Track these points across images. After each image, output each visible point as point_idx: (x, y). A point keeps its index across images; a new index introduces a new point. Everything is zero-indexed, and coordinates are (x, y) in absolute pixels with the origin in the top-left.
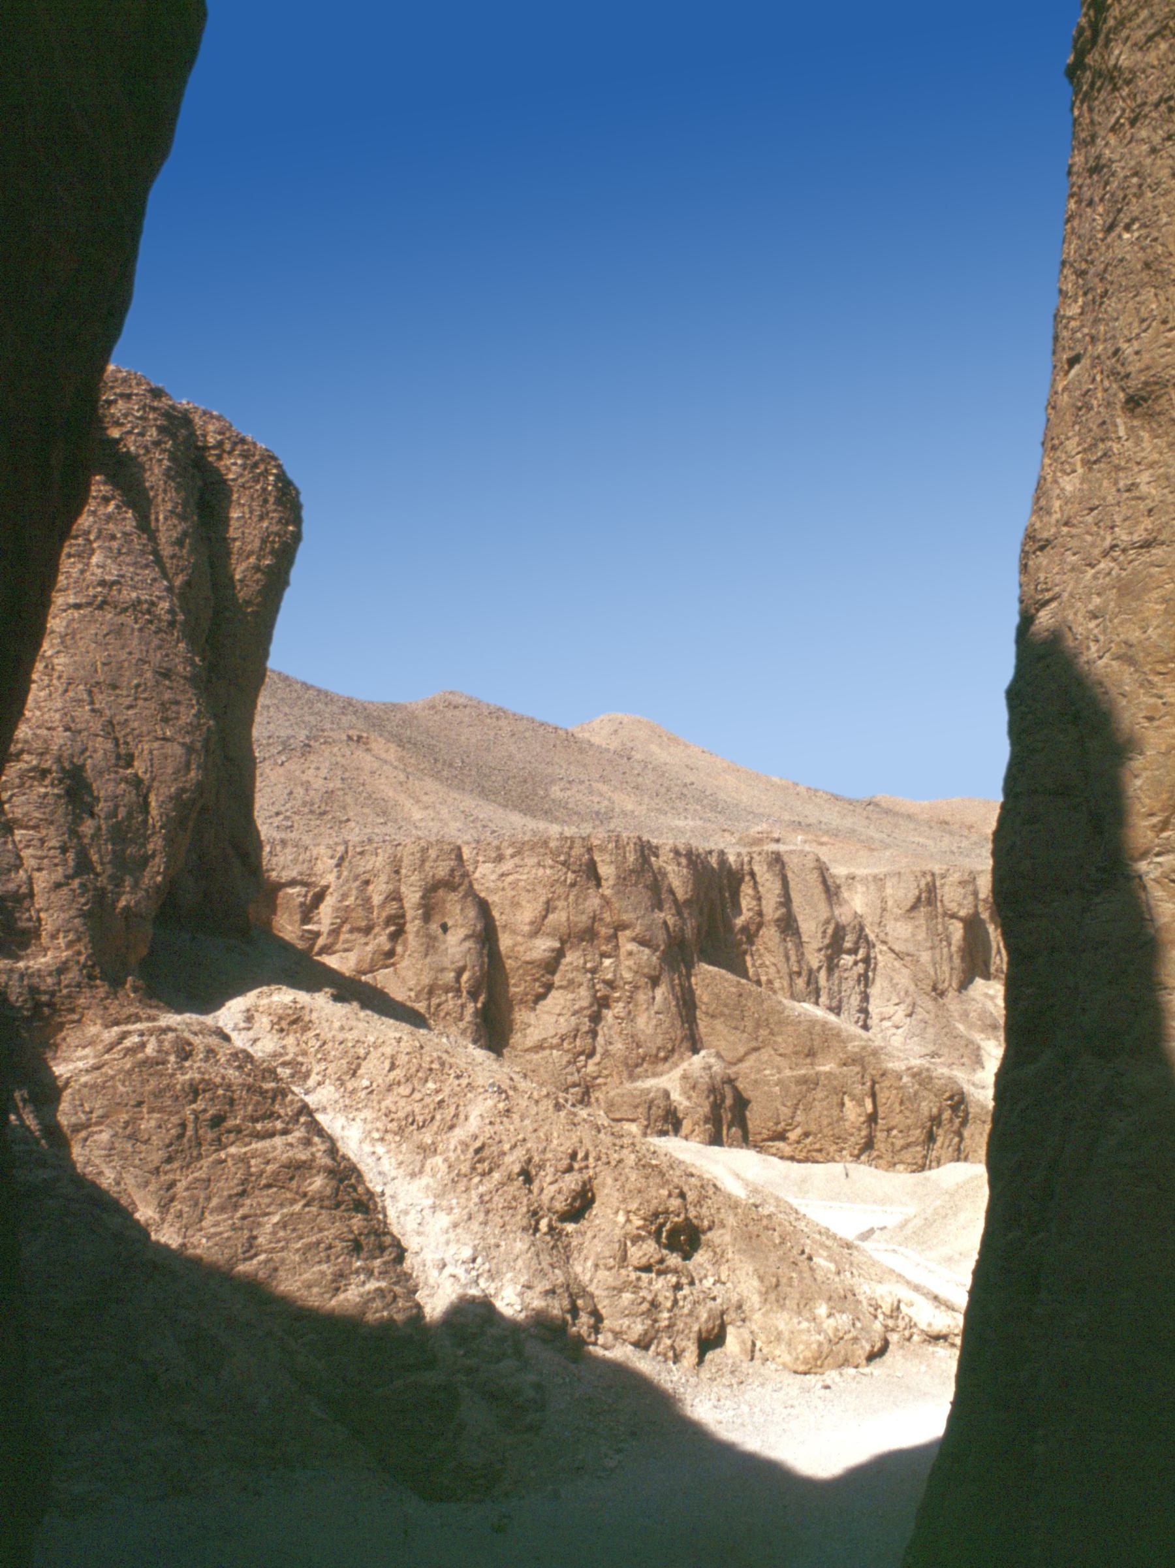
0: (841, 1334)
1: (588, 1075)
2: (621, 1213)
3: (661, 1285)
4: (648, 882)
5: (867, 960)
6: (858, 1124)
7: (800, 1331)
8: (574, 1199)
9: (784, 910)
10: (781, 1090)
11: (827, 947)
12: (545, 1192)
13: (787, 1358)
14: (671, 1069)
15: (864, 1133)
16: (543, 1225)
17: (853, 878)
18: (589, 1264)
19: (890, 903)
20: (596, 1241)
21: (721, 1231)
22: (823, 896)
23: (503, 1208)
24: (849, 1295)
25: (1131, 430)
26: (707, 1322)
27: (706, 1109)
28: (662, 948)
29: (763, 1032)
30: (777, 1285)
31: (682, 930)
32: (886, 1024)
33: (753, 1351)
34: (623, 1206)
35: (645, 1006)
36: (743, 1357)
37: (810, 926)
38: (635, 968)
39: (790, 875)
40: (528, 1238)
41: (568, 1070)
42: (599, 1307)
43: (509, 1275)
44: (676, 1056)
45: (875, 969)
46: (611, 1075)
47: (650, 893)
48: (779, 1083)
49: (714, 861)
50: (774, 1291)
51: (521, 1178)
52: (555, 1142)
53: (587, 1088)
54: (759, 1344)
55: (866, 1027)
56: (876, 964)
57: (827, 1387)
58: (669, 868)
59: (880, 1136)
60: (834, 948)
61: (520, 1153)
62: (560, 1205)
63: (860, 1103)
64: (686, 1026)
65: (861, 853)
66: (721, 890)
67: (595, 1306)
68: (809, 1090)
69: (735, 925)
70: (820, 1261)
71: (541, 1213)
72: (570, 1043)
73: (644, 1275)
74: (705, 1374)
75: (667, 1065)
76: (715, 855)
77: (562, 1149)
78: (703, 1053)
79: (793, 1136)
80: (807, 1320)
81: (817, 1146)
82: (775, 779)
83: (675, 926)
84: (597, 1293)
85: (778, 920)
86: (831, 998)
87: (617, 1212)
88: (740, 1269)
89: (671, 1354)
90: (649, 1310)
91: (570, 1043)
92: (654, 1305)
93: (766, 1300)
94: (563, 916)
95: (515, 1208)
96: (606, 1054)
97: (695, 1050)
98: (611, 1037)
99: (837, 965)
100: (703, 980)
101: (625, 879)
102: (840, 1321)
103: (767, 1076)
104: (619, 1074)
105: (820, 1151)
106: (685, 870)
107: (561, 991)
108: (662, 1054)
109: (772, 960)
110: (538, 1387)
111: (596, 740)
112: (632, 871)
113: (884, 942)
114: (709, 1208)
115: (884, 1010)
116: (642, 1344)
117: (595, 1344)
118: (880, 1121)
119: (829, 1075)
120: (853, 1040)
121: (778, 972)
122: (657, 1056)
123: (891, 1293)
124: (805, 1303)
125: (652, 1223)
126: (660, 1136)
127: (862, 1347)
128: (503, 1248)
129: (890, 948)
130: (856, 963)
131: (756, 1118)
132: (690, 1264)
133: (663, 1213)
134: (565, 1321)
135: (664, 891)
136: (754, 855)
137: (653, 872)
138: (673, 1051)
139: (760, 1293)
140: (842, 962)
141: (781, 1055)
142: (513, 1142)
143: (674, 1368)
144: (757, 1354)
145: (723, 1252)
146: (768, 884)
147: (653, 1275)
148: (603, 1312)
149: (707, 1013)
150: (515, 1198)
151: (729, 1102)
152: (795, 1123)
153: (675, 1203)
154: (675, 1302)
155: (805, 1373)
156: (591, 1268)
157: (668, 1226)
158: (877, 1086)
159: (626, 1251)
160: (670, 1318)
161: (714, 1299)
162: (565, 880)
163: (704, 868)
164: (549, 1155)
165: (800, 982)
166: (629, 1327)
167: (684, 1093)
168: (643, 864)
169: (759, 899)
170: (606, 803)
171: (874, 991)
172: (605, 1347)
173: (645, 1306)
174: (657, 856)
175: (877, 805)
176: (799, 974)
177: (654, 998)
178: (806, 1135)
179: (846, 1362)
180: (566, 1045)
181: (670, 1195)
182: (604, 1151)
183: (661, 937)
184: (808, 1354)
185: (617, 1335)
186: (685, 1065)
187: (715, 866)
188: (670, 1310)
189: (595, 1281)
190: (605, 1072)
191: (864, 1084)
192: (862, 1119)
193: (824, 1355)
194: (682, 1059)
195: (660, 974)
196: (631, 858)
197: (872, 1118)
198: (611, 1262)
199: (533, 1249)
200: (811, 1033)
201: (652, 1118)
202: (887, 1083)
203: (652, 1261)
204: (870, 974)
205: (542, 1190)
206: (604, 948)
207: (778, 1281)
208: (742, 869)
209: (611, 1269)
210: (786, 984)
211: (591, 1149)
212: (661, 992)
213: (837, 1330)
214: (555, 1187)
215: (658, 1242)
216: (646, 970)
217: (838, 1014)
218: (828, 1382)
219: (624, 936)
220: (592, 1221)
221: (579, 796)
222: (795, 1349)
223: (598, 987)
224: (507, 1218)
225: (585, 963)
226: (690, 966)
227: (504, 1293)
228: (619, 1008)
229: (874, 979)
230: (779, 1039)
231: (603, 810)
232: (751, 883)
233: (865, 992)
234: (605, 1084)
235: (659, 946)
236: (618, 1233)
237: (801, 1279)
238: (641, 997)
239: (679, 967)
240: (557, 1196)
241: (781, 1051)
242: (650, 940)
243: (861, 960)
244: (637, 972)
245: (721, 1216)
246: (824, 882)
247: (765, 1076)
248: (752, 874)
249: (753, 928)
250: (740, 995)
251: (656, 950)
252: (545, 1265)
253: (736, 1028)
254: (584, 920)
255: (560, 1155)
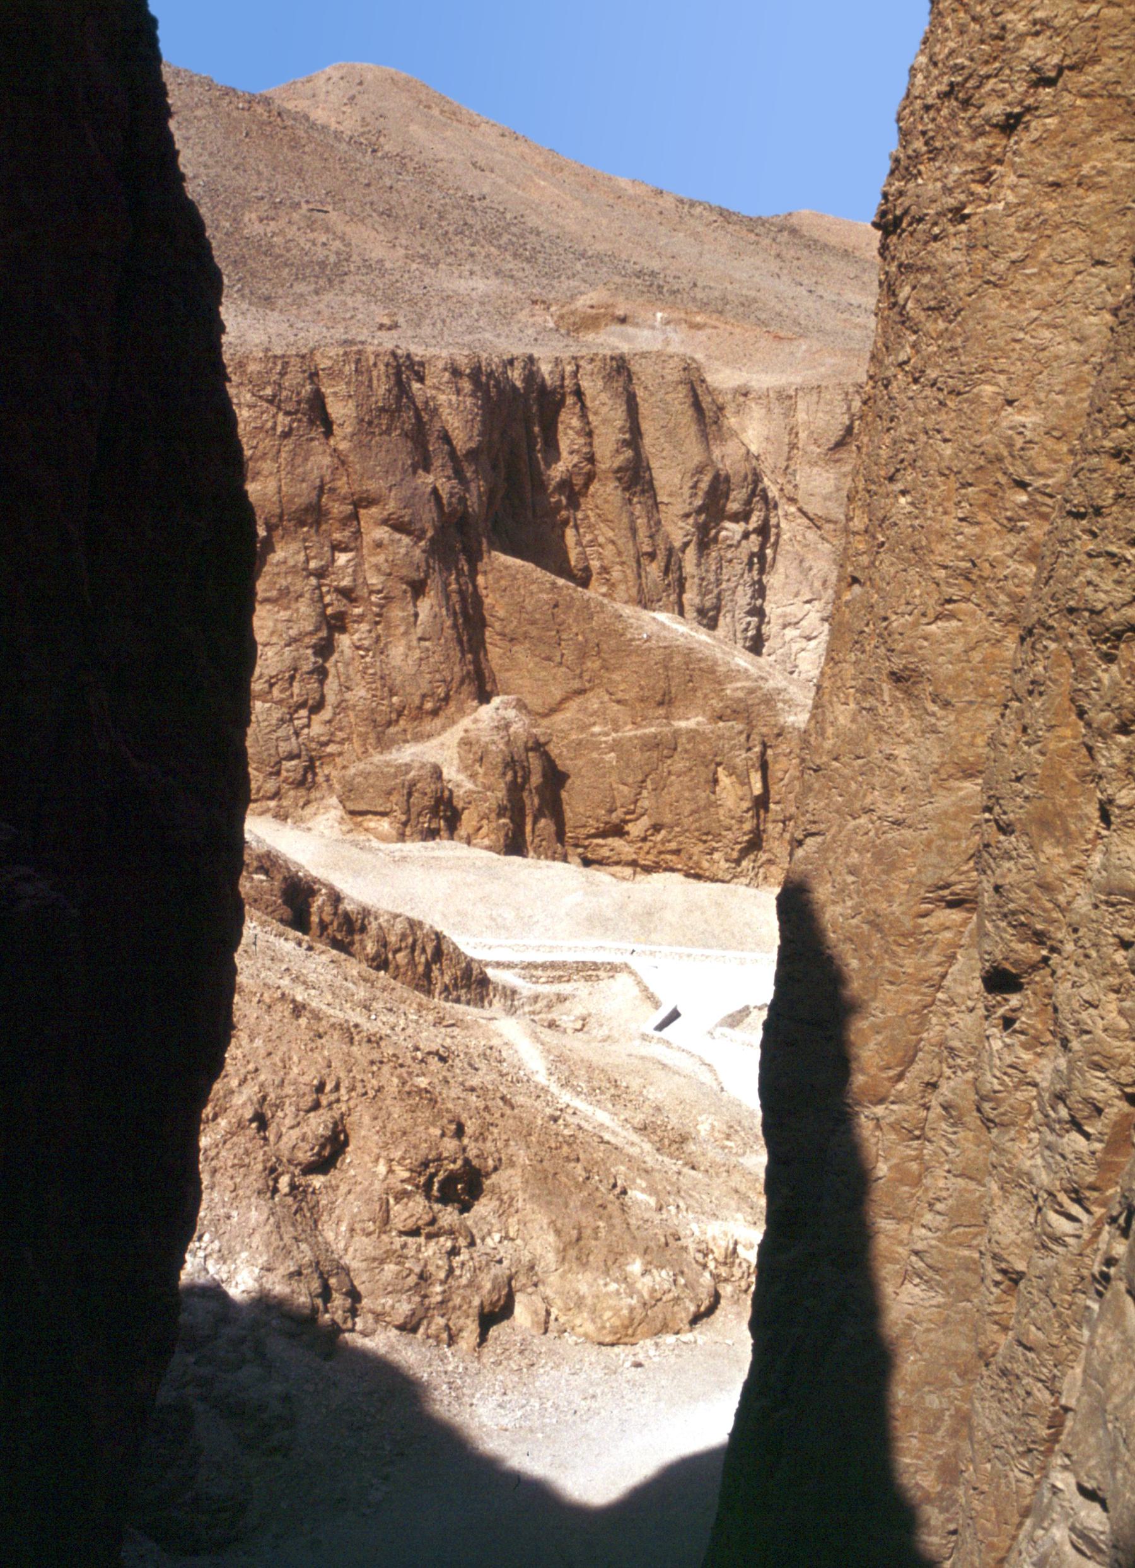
0: (658, 1295)
1: (312, 740)
2: (382, 1161)
3: (432, 1251)
4: (407, 427)
5: (763, 530)
6: (739, 813)
7: (608, 1294)
8: (323, 1147)
9: (629, 453)
10: (619, 759)
11: (699, 511)
12: (285, 1139)
13: (590, 1328)
14: (444, 728)
15: (747, 826)
16: (284, 1182)
17: (745, 395)
18: (343, 1228)
19: (803, 435)
20: (351, 1197)
21: (510, 1172)
22: (694, 428)
23: (233, 1166)
24: (671, 1240)
25: (895, 699)
26: (490, 1292)
27: (500, 794)
28: (430, 534)
29: (592, 664)
30: (579, 1239)
31: (462, 500)
32: (790, 633)
33: (547, 1322)
34: (384, 1154)
35: (402, 629)
36: (534, 1332)
37: (671, 476)
38: (385, 567)
39: (640, 393)
40: (265, 1206)
41: (280, 733)
42: (356, 1283)
43: (244, 1255)
44: (452, 708)
45: (776, 544)
46: (349, 739)
47: (410, 444)
48: (615, 746)
49: (516, 375)
50: (575, 1248)
51: (254, 1125)
52: (295, 1070)
53: (312, 760)
54: (554, 1312)
55: (756, 645)
56: (778, 535)
57: (638, 1365)
58: (442, 398)
59: (773, 829)
60: (713, 507)
61: (250, 1091)
62: (305, 1155)
63: (745, 782)
64: (469, 656)
65: (763, 343)
66: (528, 424)
67: (353, 1286)
68: (662, 759)
69: (550, 479)
70: (638, 1195)
71: (280, 1169)
72: (282, 691)
73: (410, 1240)
74: (488, 1357)
75: (438, 722)
76: (518, 365)
77: (306, 1079)
78: (496, 701)
79: (635, 829)
80: (616, 1281)
81: (673, 845)
82: (623, 182)
83: (452, 495)
84: (354, 1265)
85: (620, 469)
86: (704, 593)
87: (377, 1160)
88: (532, 1221)
89: (445, 1336)
90: (417, 1284)
91: (282, 691)
92: (424, 1277)
93: (564, 1259)
94: (272, 485)
95: (249, 1165)
96: (341, 707)
97: (484, 697)
98: (348, 678)
99: (715, 540)
100: (497, 581)
101: (370, 423)
102: (658, 1279)
103: (597, 736)
104: (364, 737)
105: (677, 852)
106: (469, 401)
107: (268, 607)
108: (429, 705)
109: (611, 534)
110: (286, 1398)
111: (320, 115)
112: (382, 410)
113: (792, 500)
114: (494, 1140)
115: (788, 609)
116: (409, 1327)
117: (352, 1330)
118: (772, 806)
119: (693, 735)
120: (733, 679)
121: (619, 554)
122: (420, 708)
123: (726, 1234)
124: (615, 1258)
125: (420, 1174)
126: (424, 840)
127: (686, 1309)
128: (235, 1220)
129: (800, 510)
130: (746, 535)
131: (577, 804)
132: (470, 1218)
133: (434, 1161)
134: (315, 1310)
135: (432, 439)
136: (582, 363)
137: (417, 410)
138: (447, 699)
139: (558, 1251)
140: (723, 533)
141: (619, 702)
142: (243, 1071)
143: (448, 1352)
144: (552, 1325)
145: (512, 1199)
146: (604, 410)
147: (422, 1240)
148: (361, 1288)
149: (502, 634)
150: (247, 1153)
151: (536, 779)
152: (639, 811)
153: (450, 1146)
154: (451, 1271)
155: (613, 1345)
156: (346, 1236)
157: (442, 1175)
158: (770, 752)
159: (388, 1211)
160: (444, 1292)
161: (500, 1262)
162: (274, 428)
163: (501, 392)
164: (289, 1090)
165: (654, 570)
166: (393, 1307)
167: (465, 768)
168: (398, 399)
169: (590, 434)
170: (337, 245)
171: (773, 580)
172: (365, 1334)
173: (412, 1280)
174: (421, 380)
175: (794, 231)
176: (652, 556)
177: (416, 615)
178: (657, 828)
179: (665, 1328)
180: (276, 692)
181: (443, 1135)
182: (359, 1077)
183: (428, 517)
184: (617, 1322)
185: (378, 1316)
186: (466, 722)
187: (519, 384)
188: (443, 1282)
189: (351, 1249)
190: (340, 735)
191: (749, 749)
192: (746, 805)
193: (636, 1322)
194: (461, 711)
195: (427, 576)
196: (382, 388)
197: (761, 803)
198: (371, 1226)
199: (272, 1220)
200: (666, 668)
201: (414, 810)
202: (784, 748)
203: (420, 1222)
204: (768, 551)
205: (280, 1136)
206: (337, 536)
207: (580, 1233)
208: (562, 386)
209: (369, 1234)
210: (631, 575)
211: (342, 1075)
212: (426, 606)
213: (654, 1290)
214: (295, 1133)
215: (428, 1197)
216: (404, 572)
217: (712, 625)
218: (641, 1358)
219: (367, 515)
220: (347, 1171)
221: (292, 232)
222: (600, 1317)
223: (327, 599)
224: (238, 1180)
225: (307, 561)
226: (474, 558)
227: (239, 1278)
228: (360, 632)
229: (774, 559)
230: (616, 677)
231: (333, 259)
232: (577, 409)
233: (760, 581)
234: (340, 754)
235: (424, 531)
236: (378, 1186)
237: (611, 1227)
238: (397, 613)
239: (457, 561)
240: (301, 1144)
241: (620, 696)
242: (410, 522)
243: (755, 531)
244: (390, 574)
245: (510, 1151)
246: (697, 405)
247: (593, 735)
248: (579, 393)
249: (578, 481)
250: (556, 606)
251: (420, 539)
252: (287, 1239)
253: (548, 659)
254: (303, 493)
255: (304, 1089)
